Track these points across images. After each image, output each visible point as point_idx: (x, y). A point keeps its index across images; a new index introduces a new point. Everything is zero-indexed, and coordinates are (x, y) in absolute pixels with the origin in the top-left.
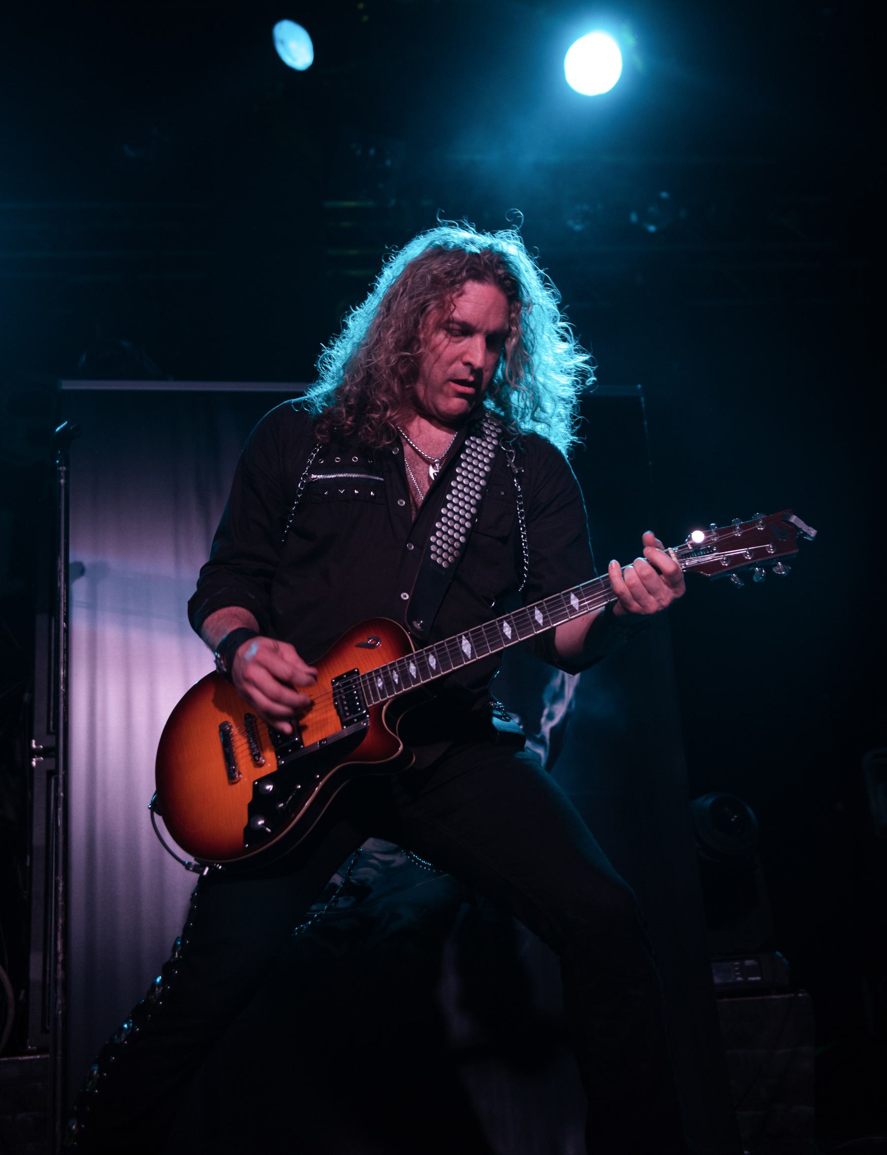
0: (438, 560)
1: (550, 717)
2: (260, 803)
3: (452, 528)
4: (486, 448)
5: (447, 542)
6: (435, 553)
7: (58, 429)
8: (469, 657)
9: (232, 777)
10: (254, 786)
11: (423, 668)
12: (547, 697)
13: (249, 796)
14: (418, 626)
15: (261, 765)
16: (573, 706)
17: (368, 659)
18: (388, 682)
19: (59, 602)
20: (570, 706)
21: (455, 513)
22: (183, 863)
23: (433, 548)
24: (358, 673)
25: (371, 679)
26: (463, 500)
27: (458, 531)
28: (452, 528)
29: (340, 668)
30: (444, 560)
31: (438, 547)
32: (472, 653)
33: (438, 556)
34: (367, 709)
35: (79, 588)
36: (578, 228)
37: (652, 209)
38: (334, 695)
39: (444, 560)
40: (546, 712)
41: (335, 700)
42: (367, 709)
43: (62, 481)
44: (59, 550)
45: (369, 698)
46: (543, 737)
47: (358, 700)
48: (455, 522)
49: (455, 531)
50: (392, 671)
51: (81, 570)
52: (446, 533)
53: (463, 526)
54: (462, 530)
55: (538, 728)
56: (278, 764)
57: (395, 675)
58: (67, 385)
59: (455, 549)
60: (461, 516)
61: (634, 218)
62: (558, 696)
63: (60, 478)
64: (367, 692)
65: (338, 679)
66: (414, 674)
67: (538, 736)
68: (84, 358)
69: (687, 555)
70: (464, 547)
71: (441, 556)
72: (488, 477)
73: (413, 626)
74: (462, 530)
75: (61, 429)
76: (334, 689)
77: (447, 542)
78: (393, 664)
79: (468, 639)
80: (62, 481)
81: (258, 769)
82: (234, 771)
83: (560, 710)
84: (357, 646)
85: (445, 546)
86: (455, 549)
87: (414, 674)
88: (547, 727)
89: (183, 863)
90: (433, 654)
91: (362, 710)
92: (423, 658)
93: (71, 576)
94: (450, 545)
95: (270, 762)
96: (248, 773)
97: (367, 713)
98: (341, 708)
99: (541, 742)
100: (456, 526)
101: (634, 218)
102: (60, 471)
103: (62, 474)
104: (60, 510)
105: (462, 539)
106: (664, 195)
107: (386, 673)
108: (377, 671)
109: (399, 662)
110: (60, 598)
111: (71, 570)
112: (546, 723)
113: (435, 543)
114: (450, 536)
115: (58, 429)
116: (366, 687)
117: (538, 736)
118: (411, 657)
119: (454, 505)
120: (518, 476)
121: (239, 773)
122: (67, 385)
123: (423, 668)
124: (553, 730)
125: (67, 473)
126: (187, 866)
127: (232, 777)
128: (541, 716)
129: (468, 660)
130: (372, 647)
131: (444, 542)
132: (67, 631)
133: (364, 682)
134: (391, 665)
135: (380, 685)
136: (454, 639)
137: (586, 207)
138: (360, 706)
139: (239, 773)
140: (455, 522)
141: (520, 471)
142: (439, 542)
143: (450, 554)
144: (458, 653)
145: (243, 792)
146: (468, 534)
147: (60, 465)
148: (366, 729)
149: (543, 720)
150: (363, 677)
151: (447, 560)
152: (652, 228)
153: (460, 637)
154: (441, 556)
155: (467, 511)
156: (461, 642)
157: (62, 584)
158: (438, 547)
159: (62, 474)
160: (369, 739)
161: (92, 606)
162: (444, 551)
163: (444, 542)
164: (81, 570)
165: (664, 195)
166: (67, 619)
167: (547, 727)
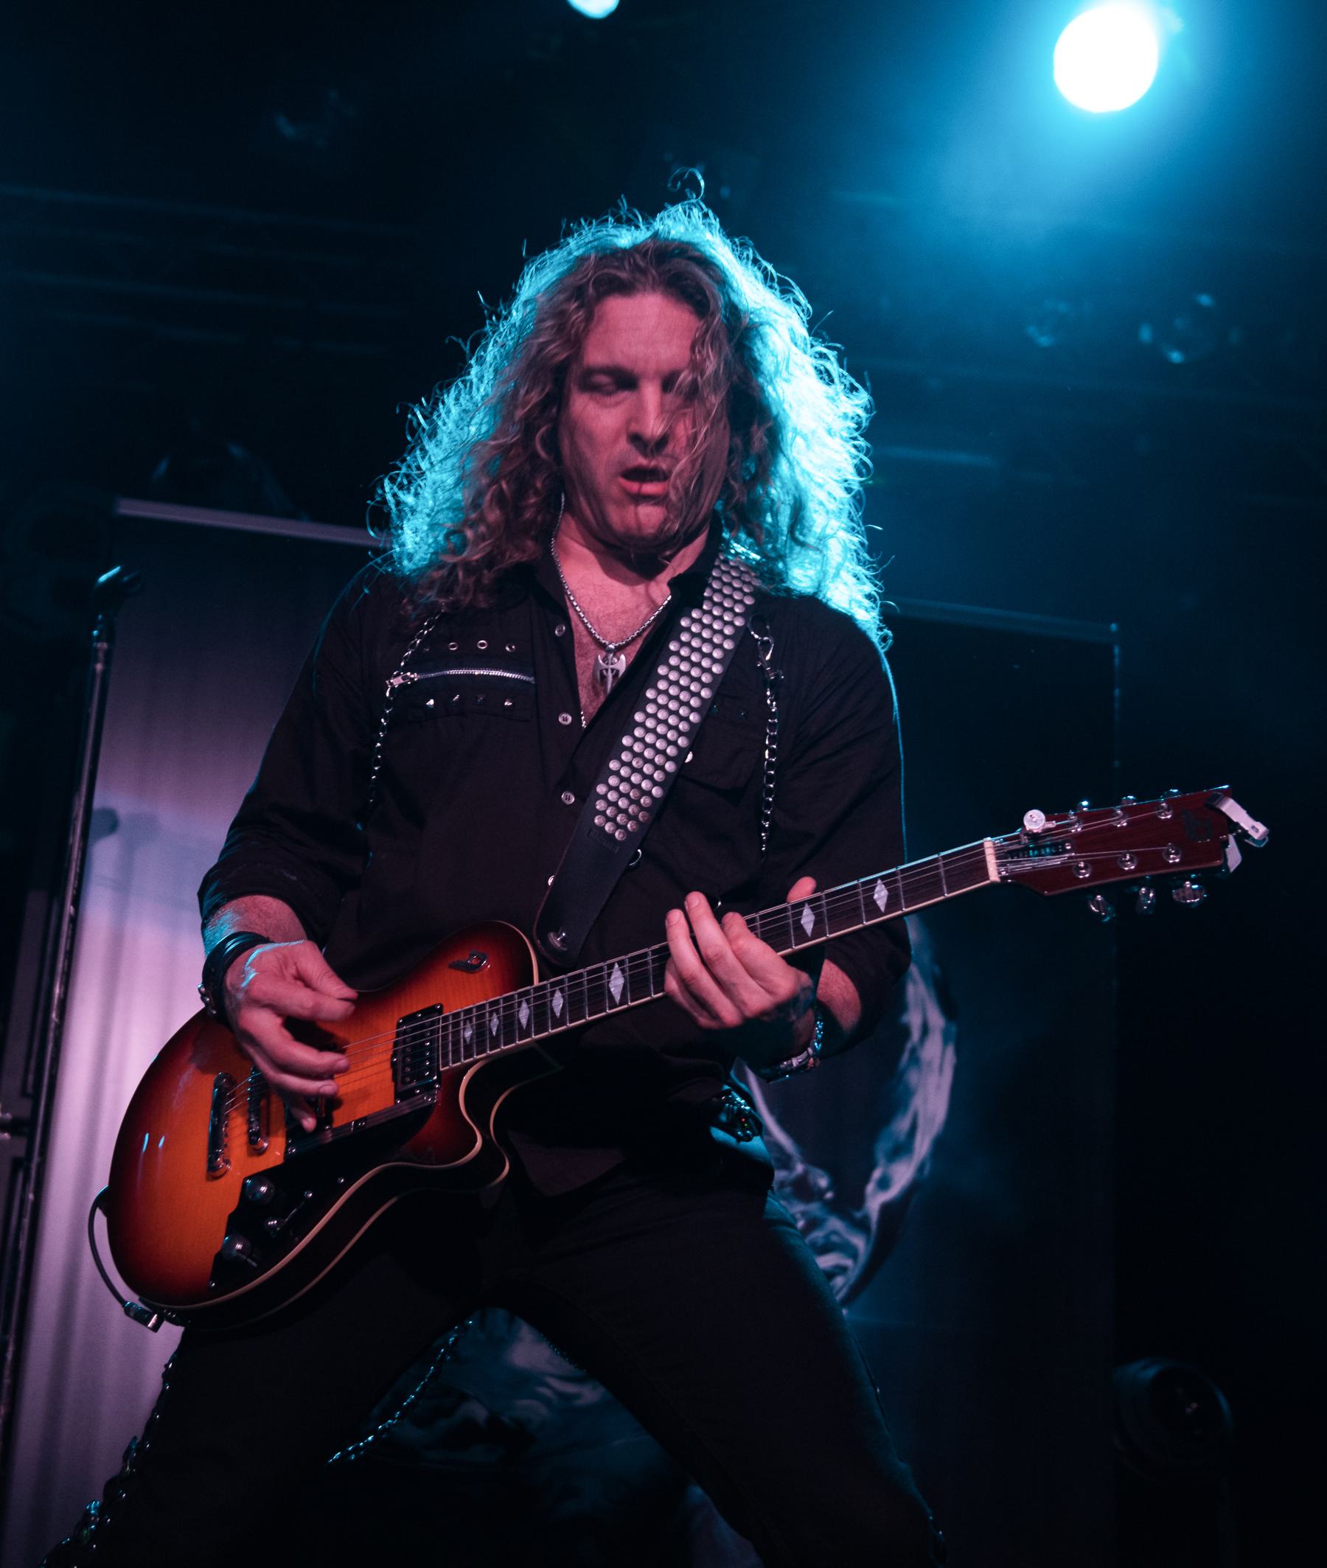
0: (608, 827)
1: (884, 1184)
2: (246, 1217)
3: (640, 771)
4: (721, 632)
5: (627, 796)
6: (603, 813)
7: (103, 578)
8: (618, 998)
9: (213, 1172)
10: (244, 1185)
11: (541, 1014)
12: (882, 1148)
13: (232, 1203)
14: (556, 941)
15: (260, 1152)
16: (926, 1171)
17: (460, 993)
18: (481, 1030)
19: (67, 871)
20: (920, 1169)
21: (647, 746)
22: (122, 1301)
23: (600, 805)
24: (440, 1011)
25: (456, 1025)
26: (665, 722)
27: (650, 777)
28: (640, 771)
29: (415, 1002)
30: (618, 826)
31: (610, 804)
32: (623, 994)
33: (608, 819)
34: (439, 1074)
35: (105, 854)
36: (1044, 341)
37: (1179, 323)
38: (396, 1044)
39: (618, 826)
40: (877, 1174)
41: (393, 1056)
42: (439, 1074)
43: (99, 667)
44: (79, 783)
45: (445, 1056)
46: (866, 1219)
47: (430, 1059)
48: (646, 761)
49: (645, 777)
50: (491, 1013)
51: (112, 824)
52: (628, 780)
53: (661, 768)
54: (658, 776)
55: (860, 1200)
56: (286, 1152)
57: (495, 1021)
58: (130, 508)
59: (642, 808)
60: (658, 752)
61: (1146, 334)
62: (901, 1150)
63: (96, 661)
64: (445, 1046)
65: (408, 1019)
66: (524, 1021)
67: (858, 1215)
68: (163, 466)
69: (1024, 851)
70: (659, 809)
71: (613, 820)
72: (719, 685)
73: (545, 941)
74: (658, 776)
75: (110, 580)
76: (398, 1034)
77: (627, 796)
78: (496, 1002)
79: (623, 971)
80: (99, 667)
81: (256, 1159)
82: (218, 1155)
83: (903, 1174)
84: (451, 967)
85: (622, 803)
86: (642, 808)
87: (524, 1021)
88: (875, 1201)
89: (122, 1301)
90: (562, 990)
91: (431, 1076)
92: (544, 996)
93: (92, 833)
94: (632, 802)
95: (275, 1151)
96: (239, 1164)
97: (438, 1081)
98: (400, 1067)
99: (861, 1225)
100: (647, 769)
101: (1146, 334)
102: (97, 650)
103: (101, 655)
104: (88, 716)
105: (656, 792)
106: (1205, 300)
107: (480, 1017)
108: (468, 1012)
109: (506, 999)
110: (70, 862)
111: (95, 822)
112: (874, 1194)
113: (604, 797)
114: (633, 786)
115: (103, 578)
116: (445, 1037)
117: (858, 1215)
118: (527, 993)
119: (648, 730)
120: (773, 686)
121: (227, 1162)
122: (130, 508)
123: (541, 1014)
124: (886, 1208)
125: (108, 654)
126: (128, 1311)
127: (213, 1172)
128: (866, 1178)
129: (613, 1005)
130: (471, 969)
131: (621, 795)
132: (75, 921)
133: (445, 1028)
134: (492, 1004)
135: (468, 1034)
136: (601, 969)
137: (1063, 307)
138: (429, 1069)
139: (227, 1162)
140: (646, 761)
141: (777, 676)
142: (612, 796)
143: (630, 817)
144: (599, 994)
145: (226, 1195)
146: (671, 783)
147: (98, 639)
148: (429, 1108)
149: (870, 1188)
150: (445, 1019)
151: (624, 827)
152: (1176, 357)
153: (611, 966)
154: (613, 820)
155: (670, 743)
156: (610, 975)
157: (76, 841)
158: (610, 804)
159: (101, 655)
160: (433, 1122)
161: (123, 887)
162: (620, 810)
163: (621, 795)
164: (112, 824)
165: (1205, 300)
166: (77, 902)
167: (875, 1201)
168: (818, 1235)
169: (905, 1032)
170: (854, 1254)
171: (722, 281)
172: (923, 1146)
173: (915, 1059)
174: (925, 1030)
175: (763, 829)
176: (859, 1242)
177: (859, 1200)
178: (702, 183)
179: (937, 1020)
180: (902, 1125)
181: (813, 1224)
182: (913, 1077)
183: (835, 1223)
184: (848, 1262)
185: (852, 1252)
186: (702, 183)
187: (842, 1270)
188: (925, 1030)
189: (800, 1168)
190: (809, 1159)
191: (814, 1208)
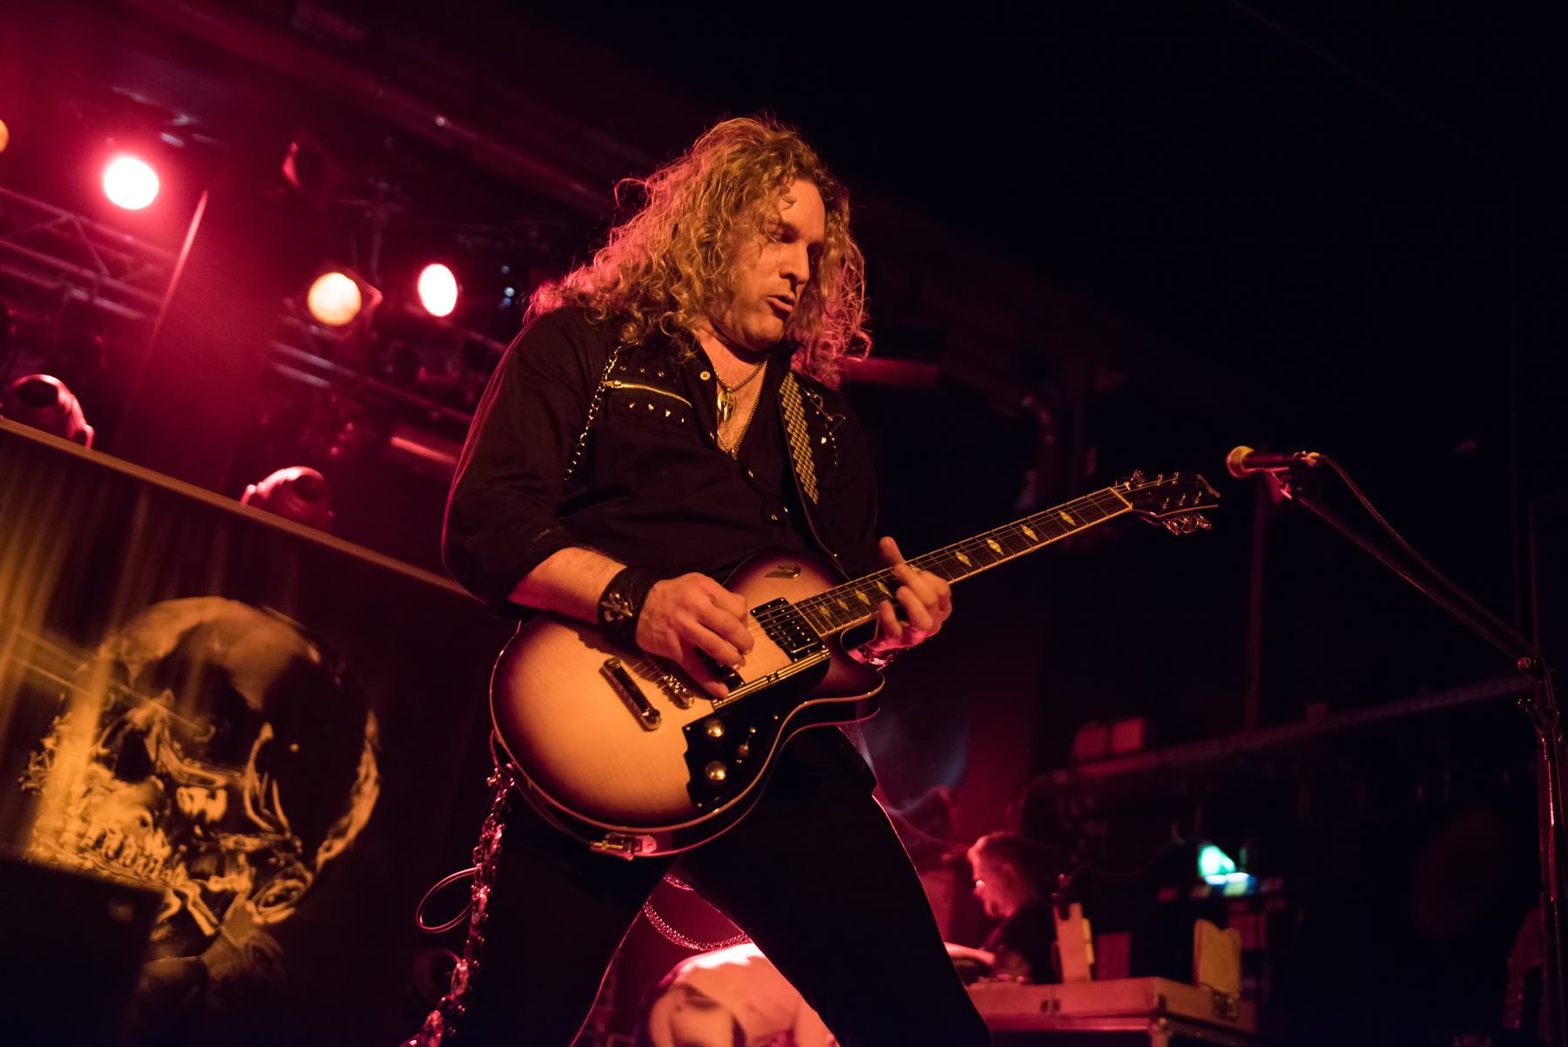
1: (328, 849)
12: (332, 830)
40: (326, 843)
62: (341, 833)
83: (339, 846)
88: (322, 857)
124: (328, 863)
128: (320, 844)
149: (321, 850)
167: (322, 857)
168: (289, 870)
169: (356, 776)
170: (302, 879)
171: (204, 768)
172: (352, 833)
173: (359, 791)
174: (367, 777)
175: (390, 276)
176: (309, 876)
177: (314, 854)
178: (362, 811)
179: (374, 773)
180: (344, 821)
181: (289, 863)
182: (355, 799)
183: (300, 865)
184: (301, 885)
185: (302, 879)
186: (362, 811)
187: (296, 889)
188: (367, 777)
189: (288, 835)
190: (295, 832)
191: (291, 856)
